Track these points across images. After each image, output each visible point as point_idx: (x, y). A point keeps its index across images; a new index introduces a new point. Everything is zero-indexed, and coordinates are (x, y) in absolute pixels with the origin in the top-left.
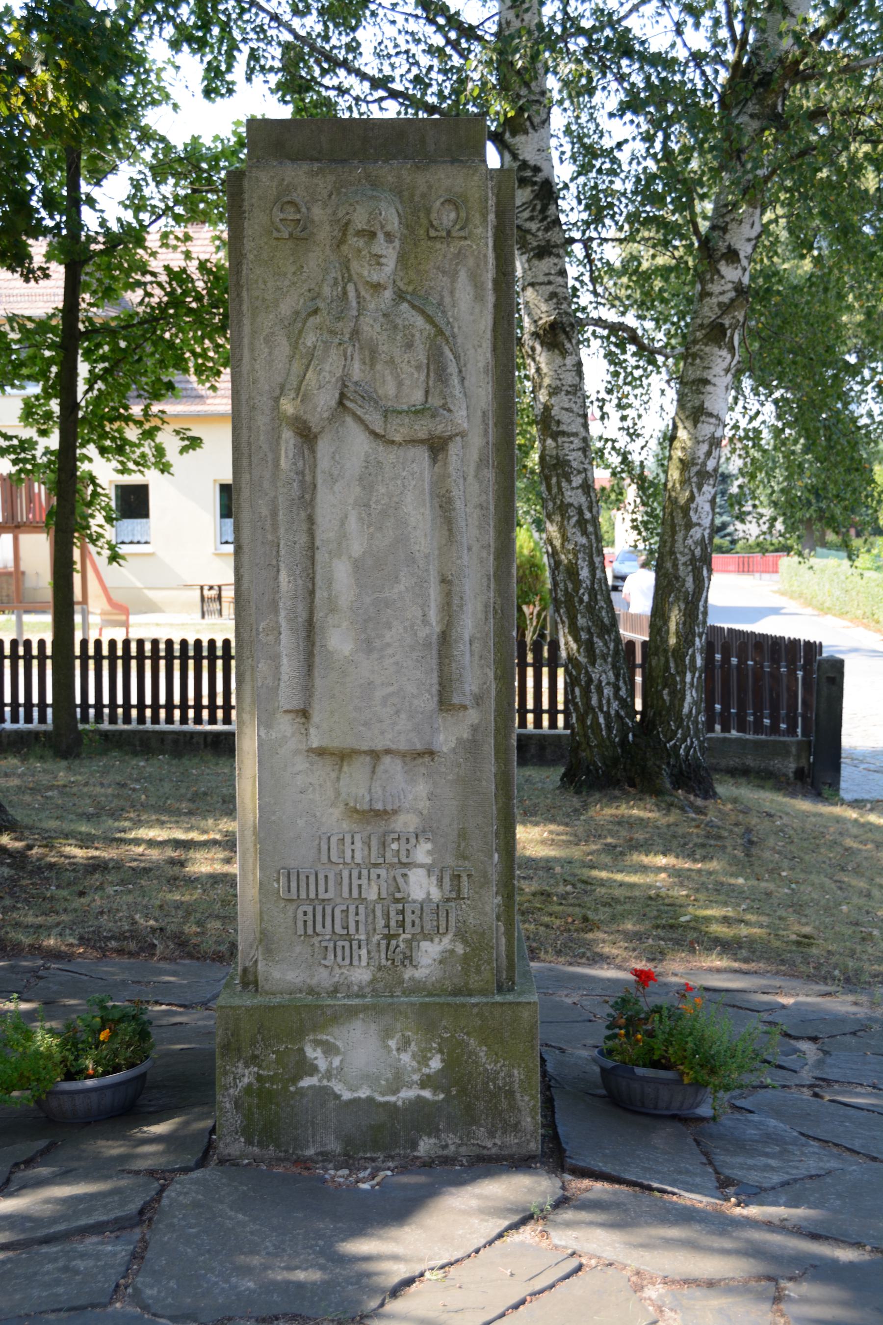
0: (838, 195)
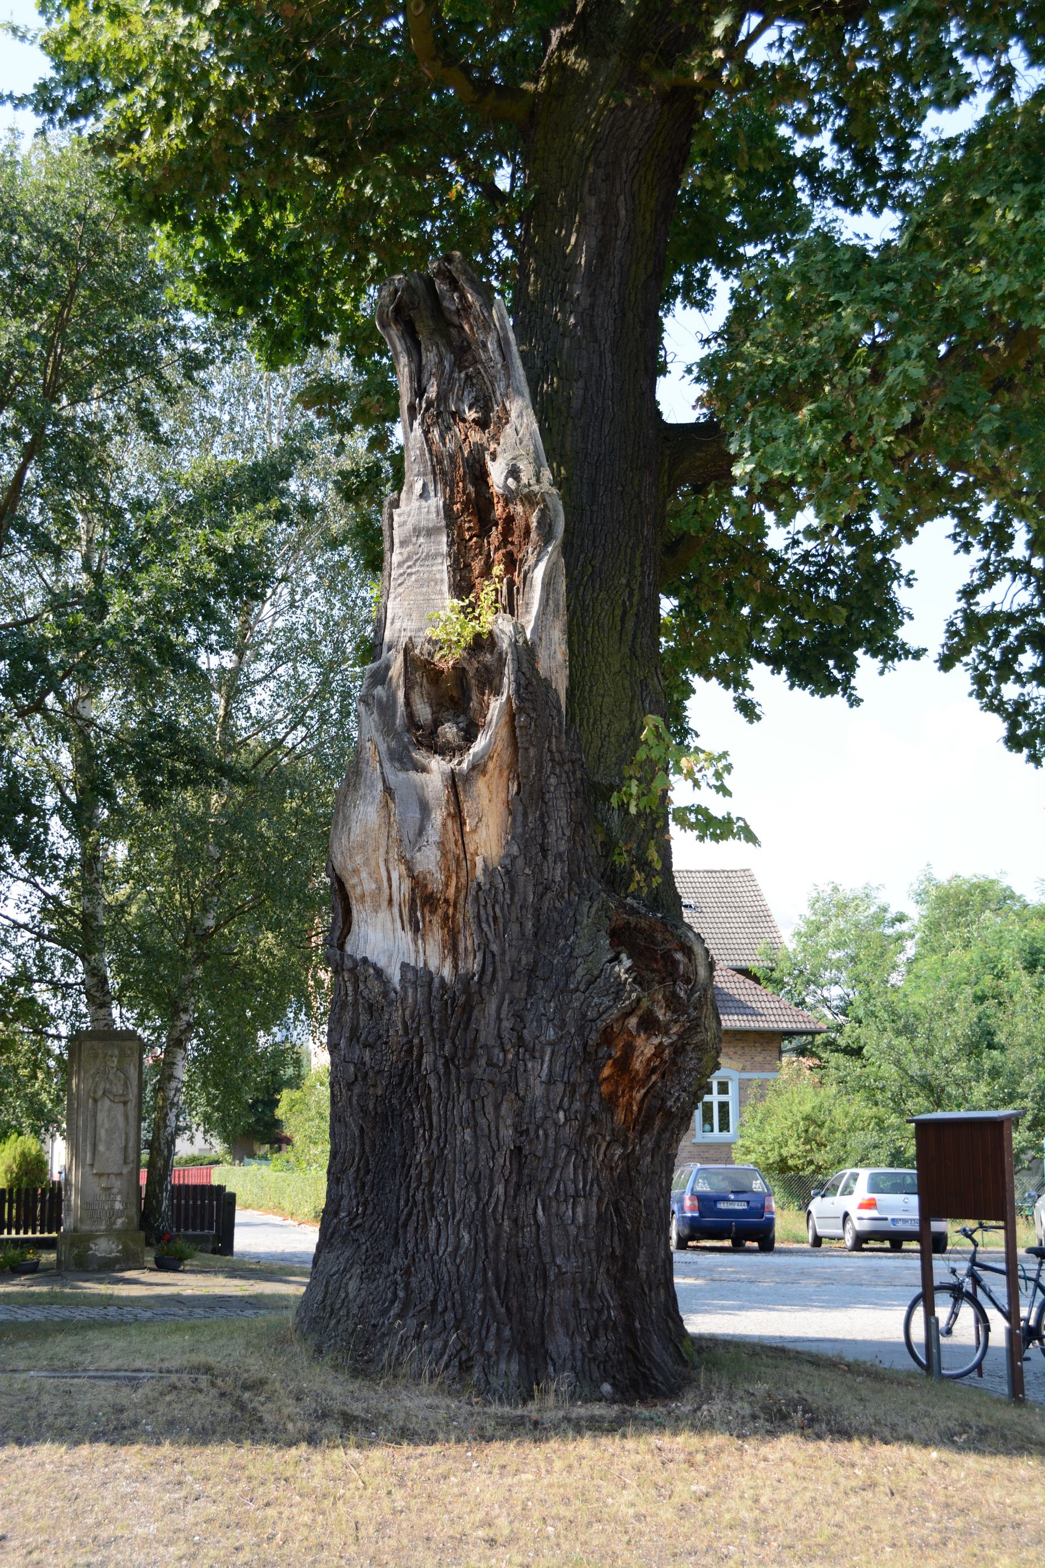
0: (641, 1534)
